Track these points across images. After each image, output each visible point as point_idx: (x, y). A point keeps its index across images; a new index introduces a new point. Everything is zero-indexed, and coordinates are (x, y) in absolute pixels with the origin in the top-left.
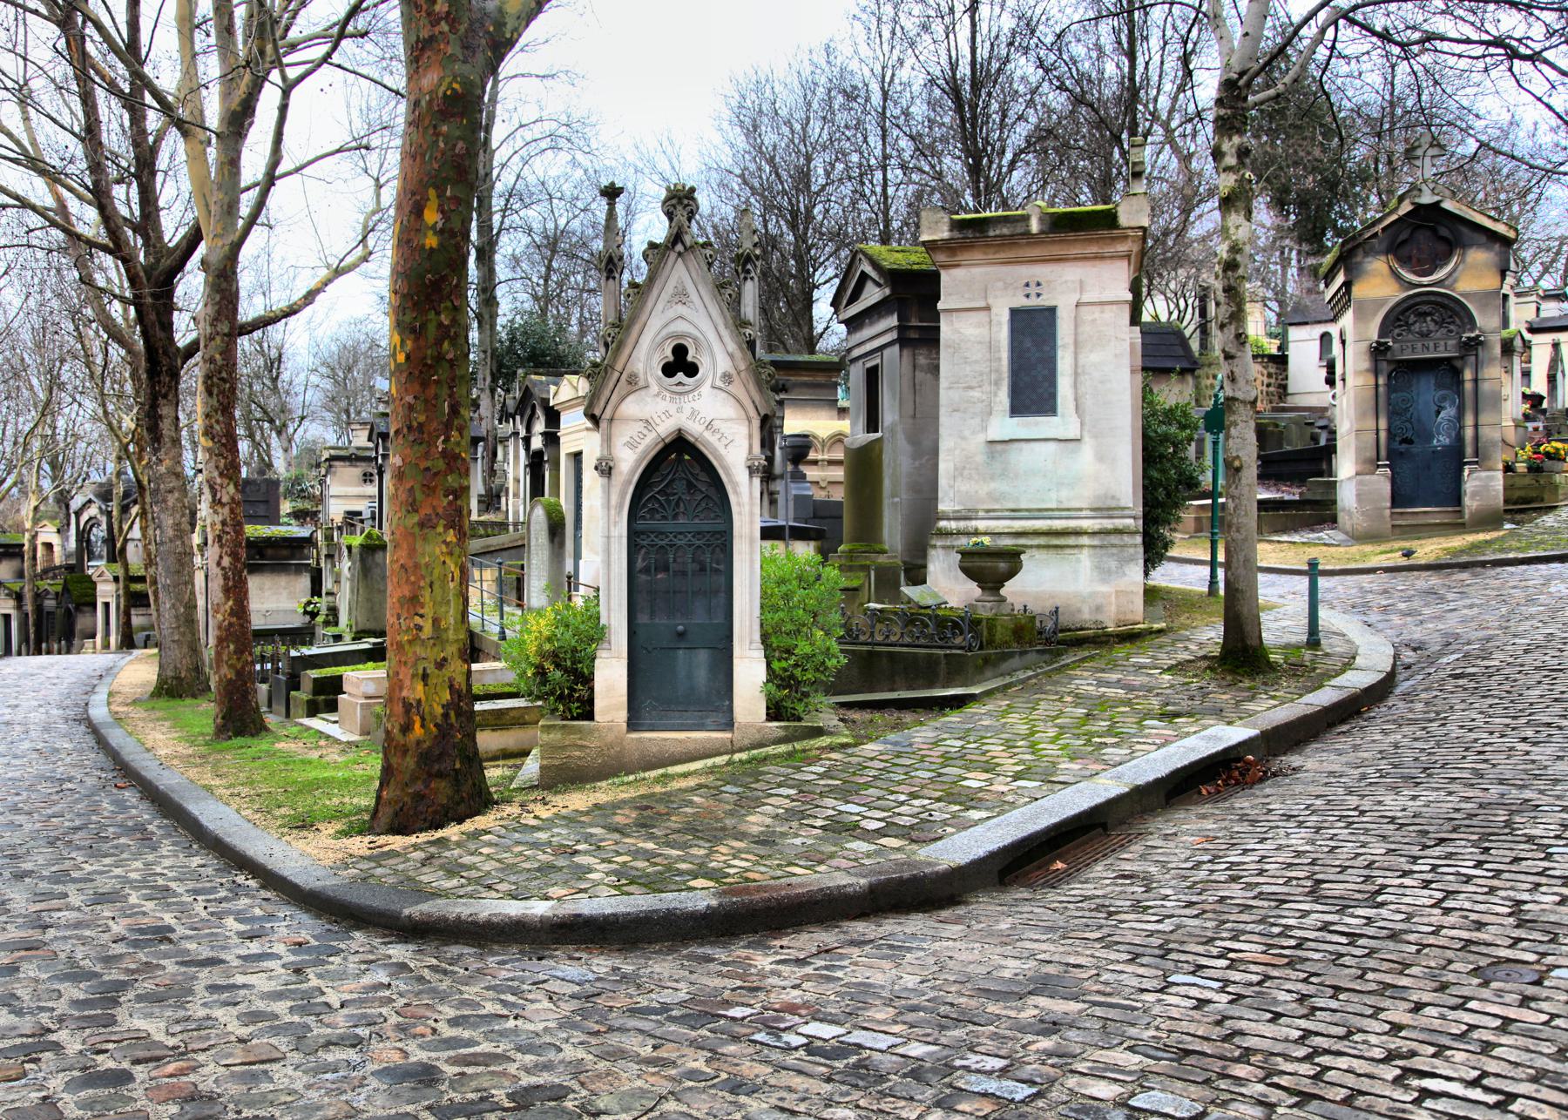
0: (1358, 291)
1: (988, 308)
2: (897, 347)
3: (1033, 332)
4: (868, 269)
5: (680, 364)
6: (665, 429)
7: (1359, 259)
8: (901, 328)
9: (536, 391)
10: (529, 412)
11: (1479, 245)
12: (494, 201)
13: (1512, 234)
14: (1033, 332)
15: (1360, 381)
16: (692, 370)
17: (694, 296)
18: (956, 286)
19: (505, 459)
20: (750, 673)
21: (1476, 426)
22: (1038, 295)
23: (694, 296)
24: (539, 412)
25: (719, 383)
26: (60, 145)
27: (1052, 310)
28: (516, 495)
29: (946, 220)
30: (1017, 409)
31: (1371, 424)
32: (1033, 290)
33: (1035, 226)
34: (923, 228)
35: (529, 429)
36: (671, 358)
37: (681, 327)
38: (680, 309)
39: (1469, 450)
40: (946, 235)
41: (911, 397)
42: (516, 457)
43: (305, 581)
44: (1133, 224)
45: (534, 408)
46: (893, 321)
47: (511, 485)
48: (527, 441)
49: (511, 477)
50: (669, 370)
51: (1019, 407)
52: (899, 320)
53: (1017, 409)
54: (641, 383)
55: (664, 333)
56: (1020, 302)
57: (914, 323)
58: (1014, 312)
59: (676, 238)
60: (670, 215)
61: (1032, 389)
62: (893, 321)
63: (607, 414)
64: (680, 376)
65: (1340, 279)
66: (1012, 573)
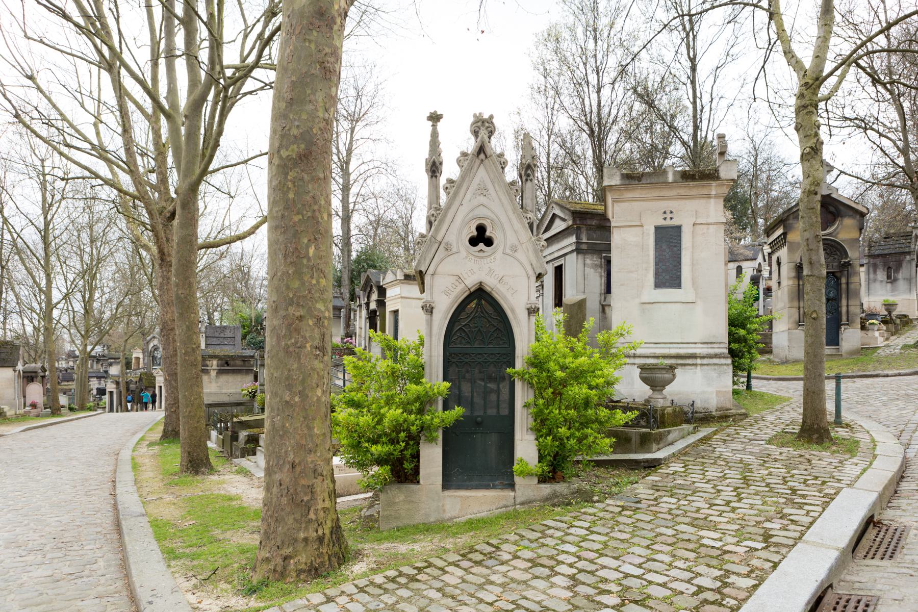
0: (790, 237)
1: (642, 226)
2: (575, 254)
3: (668, 240)
4: (557, 211)
5: (481, 238)
6: (471, 282)
7: (791, 222)
8: (578, 243)
10: (369, 289)
11: (850, 216)
12: (351, 197)
13: (865, 211)
14: (668, 240)
15: (791, 282)
16: (489, 242)
17: (492, 191)
18: (617, 213)
19: (355, 320)
21: (848, 306)
22: (671, 219)
23: (492, 191)
24: (375, 289)
26: (114, 143)
27: (679, 228)
30: (658, 285)
31: (796, 304)
32: (668, 216)
33: (670, 178)
35: (368, 298)
36: (475, 233)
37: (482, 212)
38: (482, 199)
39: (844, 318)
40: (618, 182)
43: (251, 377)
44: (728, 178)
46: (573, 239)
48: (367, 304)
49: (357, 327)
50: (473, 242)
51: (659, 284)
53: (658, 285)
54: (454, 250)
55: (471, 215)
56: (661, 223)
57: (584, 240)
58: (657, 229)
59: (481, 150)
60: (476, 133)
61: (668, 273)
62: (573, 239)
64: (481, 246)
65: (780, 231)
66: (670, 381)
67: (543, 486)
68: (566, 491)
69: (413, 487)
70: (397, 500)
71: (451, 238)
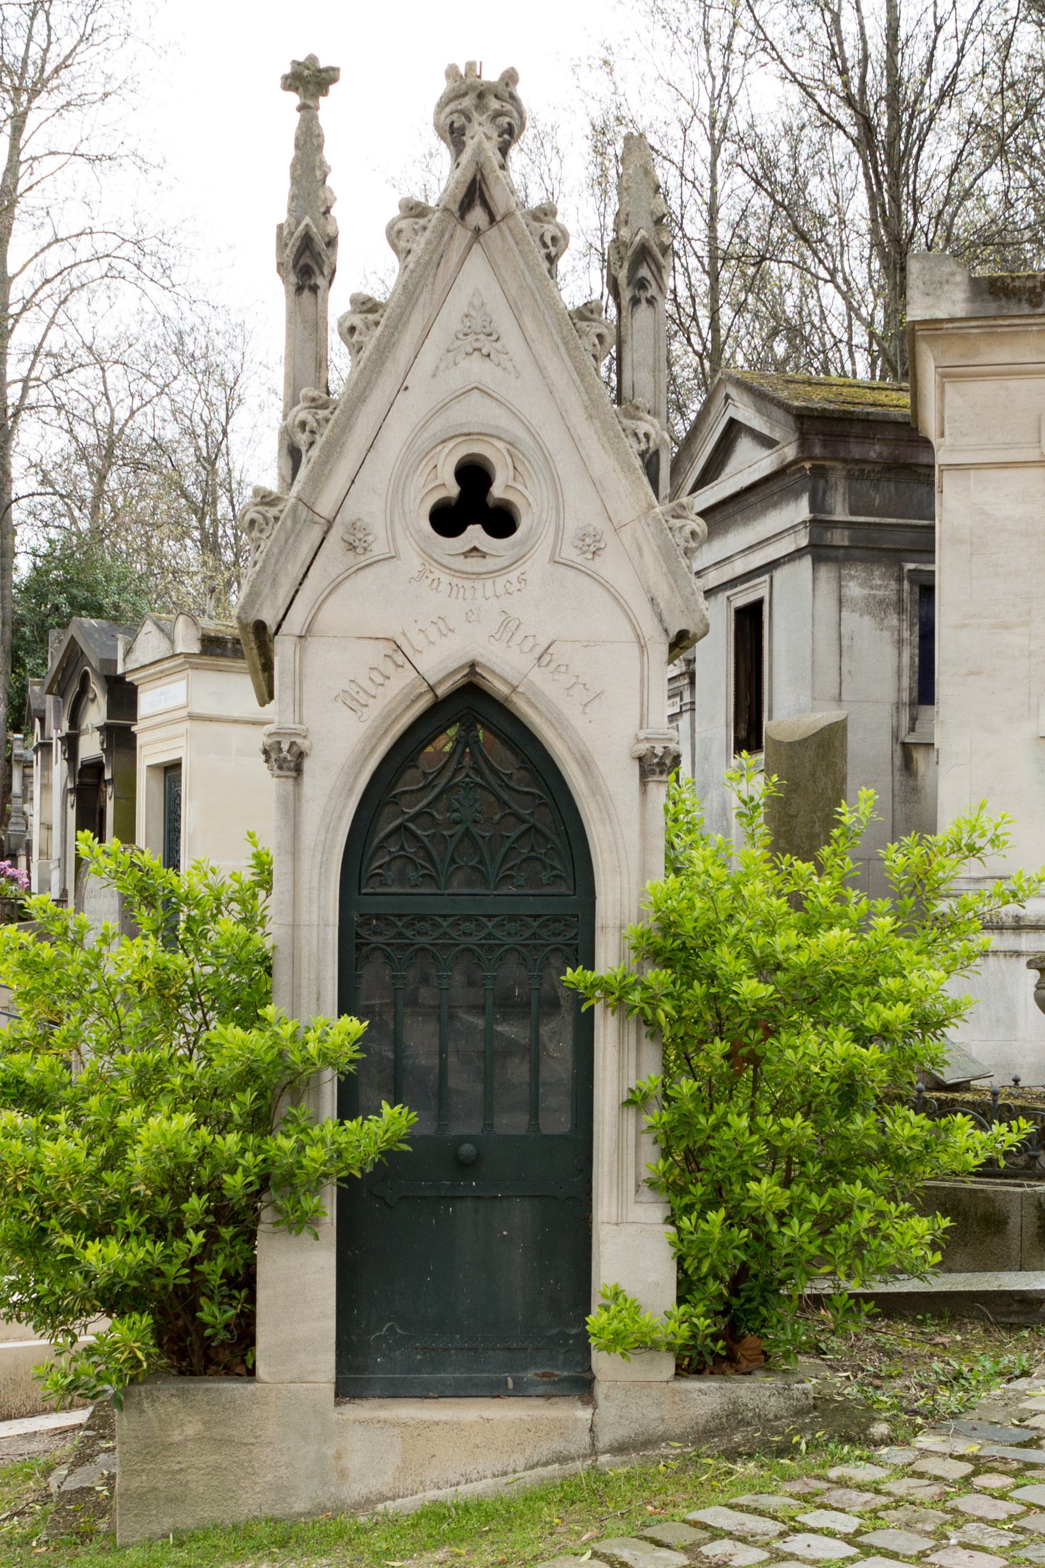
4: (745, 412)
5: (473, 506)
6: (439, 663)
8: (818, 524)
9: (93, 656)
10: (75, 688)
12: (11, 360)
16: (502, 522)
17: (511, 339)
20: (633, 1254)
23: (511, 339)
24: (96, 688)
25: (569, 553)
28: (44, 853)
29: (960, 278)
34: (913, 294)
35: (75, 720)
36: (453, 490)
37: (476, 413)
38: (477, 369)
40: (960, 309)
41: (832, 661)
42: (46, 787)
45: (85, 677)
46: (800, 510)
47: (36, 835)
48: (71, 743)
49: (35, 822)
50: (447, 520)
52: (813, 507)
54: (379, 549)
55: (437, 426)
59: (474, 194)
60: (455, 135)
62: (800, 510)
63: (295, 622)
67: (692, 1385)
68: (774, 1405)
69: (233, 1389)
70: (176, 1437)
71: (369, 506)
